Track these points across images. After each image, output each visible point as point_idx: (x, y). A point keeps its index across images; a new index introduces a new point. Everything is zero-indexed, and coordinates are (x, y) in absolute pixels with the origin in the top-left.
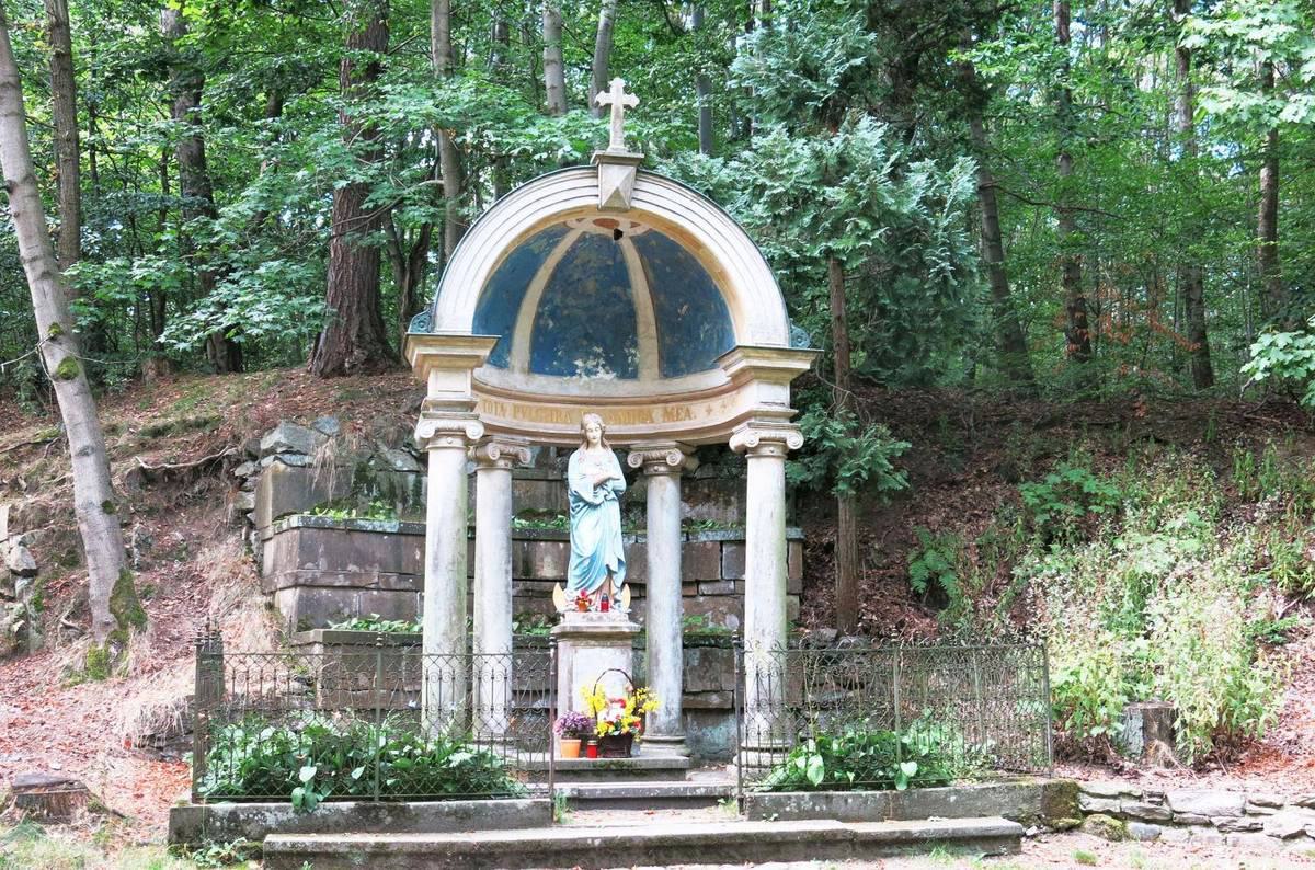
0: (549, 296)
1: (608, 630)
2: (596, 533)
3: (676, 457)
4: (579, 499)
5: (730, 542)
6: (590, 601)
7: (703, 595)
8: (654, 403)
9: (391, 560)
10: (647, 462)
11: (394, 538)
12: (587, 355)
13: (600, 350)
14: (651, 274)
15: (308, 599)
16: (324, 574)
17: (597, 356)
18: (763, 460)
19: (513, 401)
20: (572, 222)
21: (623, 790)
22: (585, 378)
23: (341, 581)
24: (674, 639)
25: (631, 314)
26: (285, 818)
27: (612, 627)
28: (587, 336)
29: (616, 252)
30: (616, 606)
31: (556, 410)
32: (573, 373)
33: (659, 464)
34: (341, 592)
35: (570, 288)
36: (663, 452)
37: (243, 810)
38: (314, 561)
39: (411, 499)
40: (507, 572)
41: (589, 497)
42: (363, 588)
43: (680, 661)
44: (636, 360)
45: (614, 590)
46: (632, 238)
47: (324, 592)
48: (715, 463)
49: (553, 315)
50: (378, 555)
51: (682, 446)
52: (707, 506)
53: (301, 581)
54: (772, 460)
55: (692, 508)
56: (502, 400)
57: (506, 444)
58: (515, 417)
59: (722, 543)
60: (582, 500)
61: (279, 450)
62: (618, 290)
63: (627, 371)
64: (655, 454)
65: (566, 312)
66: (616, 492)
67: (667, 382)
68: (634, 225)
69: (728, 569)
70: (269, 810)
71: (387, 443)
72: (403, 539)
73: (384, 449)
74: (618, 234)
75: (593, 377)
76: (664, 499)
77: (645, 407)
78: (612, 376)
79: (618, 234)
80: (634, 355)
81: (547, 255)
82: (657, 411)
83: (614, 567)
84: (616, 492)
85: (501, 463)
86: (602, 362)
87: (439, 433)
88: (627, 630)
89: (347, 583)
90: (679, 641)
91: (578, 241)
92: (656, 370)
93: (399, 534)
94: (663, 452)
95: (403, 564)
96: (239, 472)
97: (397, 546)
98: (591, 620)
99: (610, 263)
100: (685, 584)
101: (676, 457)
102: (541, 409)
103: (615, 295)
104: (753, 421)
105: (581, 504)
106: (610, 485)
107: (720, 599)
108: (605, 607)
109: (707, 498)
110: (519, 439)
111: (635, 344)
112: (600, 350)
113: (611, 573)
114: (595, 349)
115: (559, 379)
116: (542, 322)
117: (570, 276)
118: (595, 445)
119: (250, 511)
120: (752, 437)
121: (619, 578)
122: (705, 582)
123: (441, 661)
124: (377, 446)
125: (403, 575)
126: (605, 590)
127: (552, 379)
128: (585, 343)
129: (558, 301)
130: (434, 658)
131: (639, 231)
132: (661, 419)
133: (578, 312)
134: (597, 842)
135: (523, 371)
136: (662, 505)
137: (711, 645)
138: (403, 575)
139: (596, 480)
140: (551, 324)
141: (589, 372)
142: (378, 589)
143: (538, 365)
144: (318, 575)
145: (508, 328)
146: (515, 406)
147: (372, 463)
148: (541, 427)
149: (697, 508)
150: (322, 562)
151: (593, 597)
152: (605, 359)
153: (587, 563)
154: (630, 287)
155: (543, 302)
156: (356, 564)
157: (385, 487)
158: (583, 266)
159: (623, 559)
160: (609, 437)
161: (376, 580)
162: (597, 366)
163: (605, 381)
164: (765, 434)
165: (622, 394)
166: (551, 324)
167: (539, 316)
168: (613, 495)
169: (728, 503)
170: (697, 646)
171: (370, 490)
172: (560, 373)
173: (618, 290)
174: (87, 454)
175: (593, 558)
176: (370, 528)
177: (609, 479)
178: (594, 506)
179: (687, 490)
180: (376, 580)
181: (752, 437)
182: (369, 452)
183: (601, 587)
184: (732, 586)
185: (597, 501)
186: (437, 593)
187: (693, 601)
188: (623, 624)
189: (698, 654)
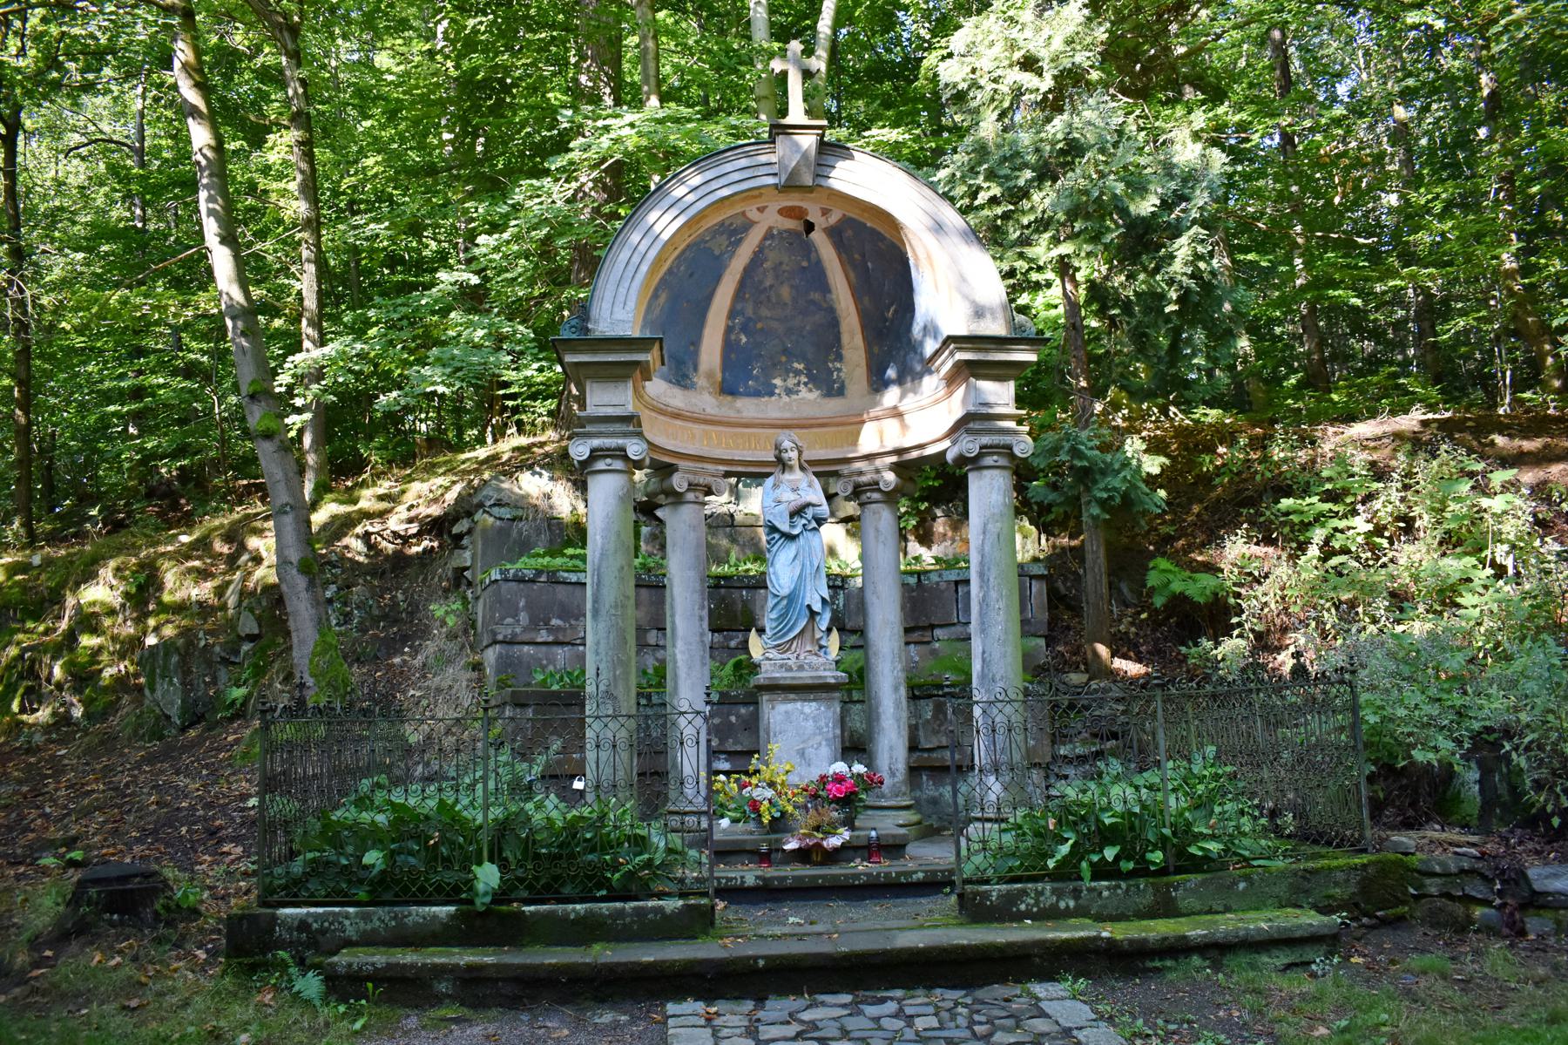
0: (739, 307)
12: (787, 372)
13: (801, 367)
14: (852, 275)
15: (508, 656)
16: (525, 629)
17: (797, 373)
18: (986, 472)
19: (703, 426)
20: (753, 214)
21: (820, 876)
22: (785, 399)
23: (543, 636)
24: (896, 689)
25: (834, 323)
26: (369, 927)
28: (785, 351)
29: (808, 249)
32: (772, 394)
34: (544, 648)
35: (763, 297)
37: (316, 916)
38: (515, 616)
40: (701, 619)
42: (568, 644)
43: (905, 714)
46: (825, 230)
47: (526, 648)
49: (744, 329)
53: (500, 637)
54: (996, 472)
56: (690, 425)
57: (695, 473)
61: (488, 503)
62: (815, 296)
65: (759, 326)
68: (825, 212)
70: (347, 916)
74: (810, 227)
78: (815, 394)
79: (810, 227)
80: (839, 370)
81: (731, 258)
83: (817, 607)
87: (595, 454)
89: (551, 639)
90: (903, 691)
91: (765, 238)
96: (456, 530)
99: (805, 264)
103: (813, 302)
104: (971, 425)
105: (777, 536)
106: (810, 512)
110: (710, 467)
111: (839, 358)
112: (801, 367)
113: (813, 614)
114: (796, 365)
115: (754, 400)
116: (733, 337)
117: (761, 282)
119: (466, 569)
120: (971, 446)
123: (1008, 709)
128: (784, 359)
129: (749, 312)
130: (690, 717)
131: (834, 219)
133: (775, 325)
134: (761, 963)
136: (876, 538)
139: (793, 506)
140: (744, 339)
141: (789, 392)
143: (727, 389)
144: (518, 630)
145: (693, 344)
148: (738, 455)
150: (524, 617)
154: (830, 291)
155: (732, 314)
156: (560, 617)
158: (774, 269)
160: (812, 463)
162: (798, 384)
166: (744, 339)
167: (729, 330)
172: (757, 394)
173: (815, 296)
174: (286, 513)
175: (792, 598)
177: (809, 505)
178: (791, 538)
181: (971, 446)
185: (795, 532)
186: (598, 643)
188: (827, 674)
189: (931, 707)
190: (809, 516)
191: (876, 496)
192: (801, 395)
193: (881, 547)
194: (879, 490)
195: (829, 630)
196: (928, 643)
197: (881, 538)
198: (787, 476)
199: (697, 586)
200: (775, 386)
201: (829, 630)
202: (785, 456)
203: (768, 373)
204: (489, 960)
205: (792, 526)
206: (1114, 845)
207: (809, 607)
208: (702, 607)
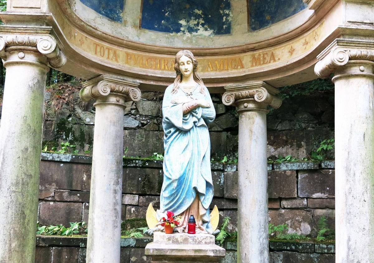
1: (192, 254)
2: (186, 158)
3: (262, 95)
4: (171, 125)
5: (304, 171)
6: (176, 223)
7: (284, 208)
8: (244, 51)
9: (65, 180)
10: (238, 101)
11: (68, 165)
12: (189, 16)
17: (197, 17)
19: (126, 50)
22: (188, 34)
27: (196, 251)
30: (204, 227)
31: (164, 59)
32: (178, 31)
33: (248, 102)
36: (251, 91)
39: (85, 138)
41: (178, 123)
44: (230, 19)
45: (202, 212)
48: (290, 121)
50: (56, 177)
51: (268, 85)
52: (285, 148)
55: (276, 149)
56: (115, 47)
57: (116, 83)
58: (127, 63)
59: (297, 171)
60: (172, 126)
63: (221, 27)
64: (244, 93)
66: (206, 119)
67: (255, 33)
69: (302, 190)
71: (80, 107)
72: (75, 167)
73: (79, 111)
75: (194, 33)
76: (252, 132)
77: (237, 56)
78: (209, 32)
80: (228, 15)
82: (247, 58)
83: (202, 189)
84: (206, 119)
85: (113, 99)
86: (202, 21)
88: (212, 254)
92: (246, 25)
93: (72, 162)
94: (251, 91)
95: (74, 184)
97: (70, 171)
98: (176, 242)
100: (271, 200)
101: (262, 95)
102: (150, 58)
105: (172, 130)
106: (200, 112)
107: (297, 212)
108: (192, 229)
109: (285, 143)
110: (130, 80)
113: (198, 195)
115: (166, 35)
118: (187, 77)
121: (207, 200)
122: (286, 199)
124: (74, 109)
125: (73, 191)
126: (193, 212)
127: (160, 34)
132: (250, 64)
135: (134, 26)
136: (250, 137)
137: (291, 250)
138: (73, 191)
139: (185, 107)
141: (191, 30)
142: (54, 201)
146: (128, 54)
147: (70, 119)
148: (150, 72)
149: (279, 150)
151: (180, 220)
152: (204, 19)
153: (175, 184)
157: (77, 134)
159: (211, 181)
161: (53, 194)
162: (198, 25)
163: (205, 36)
164: (355, 52)
165: (217, 45)
168: (202, 122)
169: (299, 146)
170: (281, 250)
171: (67, 136)
172: (166, 30)
175: (181, 181)
176: (50, 158)
177: (198, 106)
178: (184, 132)
179: (272, 138)
180: (53, 194)
181: (341, 56)
182: (68, 113)
183: (189, 209)
184: (305, 202)
185: (187, 127)
187: (277, 212)
189: (282, 256)
190: (199, 116)
191: (251, 106)
192: (199, 32)
193: (253, 143)
194: (254, 102)
195: (211, 209)
196: (277, 209)
197: (254, 137)
198: (184, 84)
199: (114, 167)
200: (181, 25)
201: (211, 209)
202: (182, 68)
203: (176, 16)
204: (280, 77)
205: (185, 121)
206: (295, 248)
207: (195, 189)
208: (117, 183)
